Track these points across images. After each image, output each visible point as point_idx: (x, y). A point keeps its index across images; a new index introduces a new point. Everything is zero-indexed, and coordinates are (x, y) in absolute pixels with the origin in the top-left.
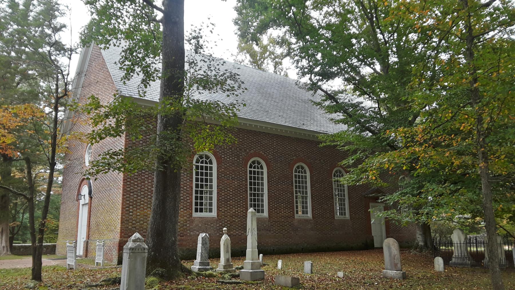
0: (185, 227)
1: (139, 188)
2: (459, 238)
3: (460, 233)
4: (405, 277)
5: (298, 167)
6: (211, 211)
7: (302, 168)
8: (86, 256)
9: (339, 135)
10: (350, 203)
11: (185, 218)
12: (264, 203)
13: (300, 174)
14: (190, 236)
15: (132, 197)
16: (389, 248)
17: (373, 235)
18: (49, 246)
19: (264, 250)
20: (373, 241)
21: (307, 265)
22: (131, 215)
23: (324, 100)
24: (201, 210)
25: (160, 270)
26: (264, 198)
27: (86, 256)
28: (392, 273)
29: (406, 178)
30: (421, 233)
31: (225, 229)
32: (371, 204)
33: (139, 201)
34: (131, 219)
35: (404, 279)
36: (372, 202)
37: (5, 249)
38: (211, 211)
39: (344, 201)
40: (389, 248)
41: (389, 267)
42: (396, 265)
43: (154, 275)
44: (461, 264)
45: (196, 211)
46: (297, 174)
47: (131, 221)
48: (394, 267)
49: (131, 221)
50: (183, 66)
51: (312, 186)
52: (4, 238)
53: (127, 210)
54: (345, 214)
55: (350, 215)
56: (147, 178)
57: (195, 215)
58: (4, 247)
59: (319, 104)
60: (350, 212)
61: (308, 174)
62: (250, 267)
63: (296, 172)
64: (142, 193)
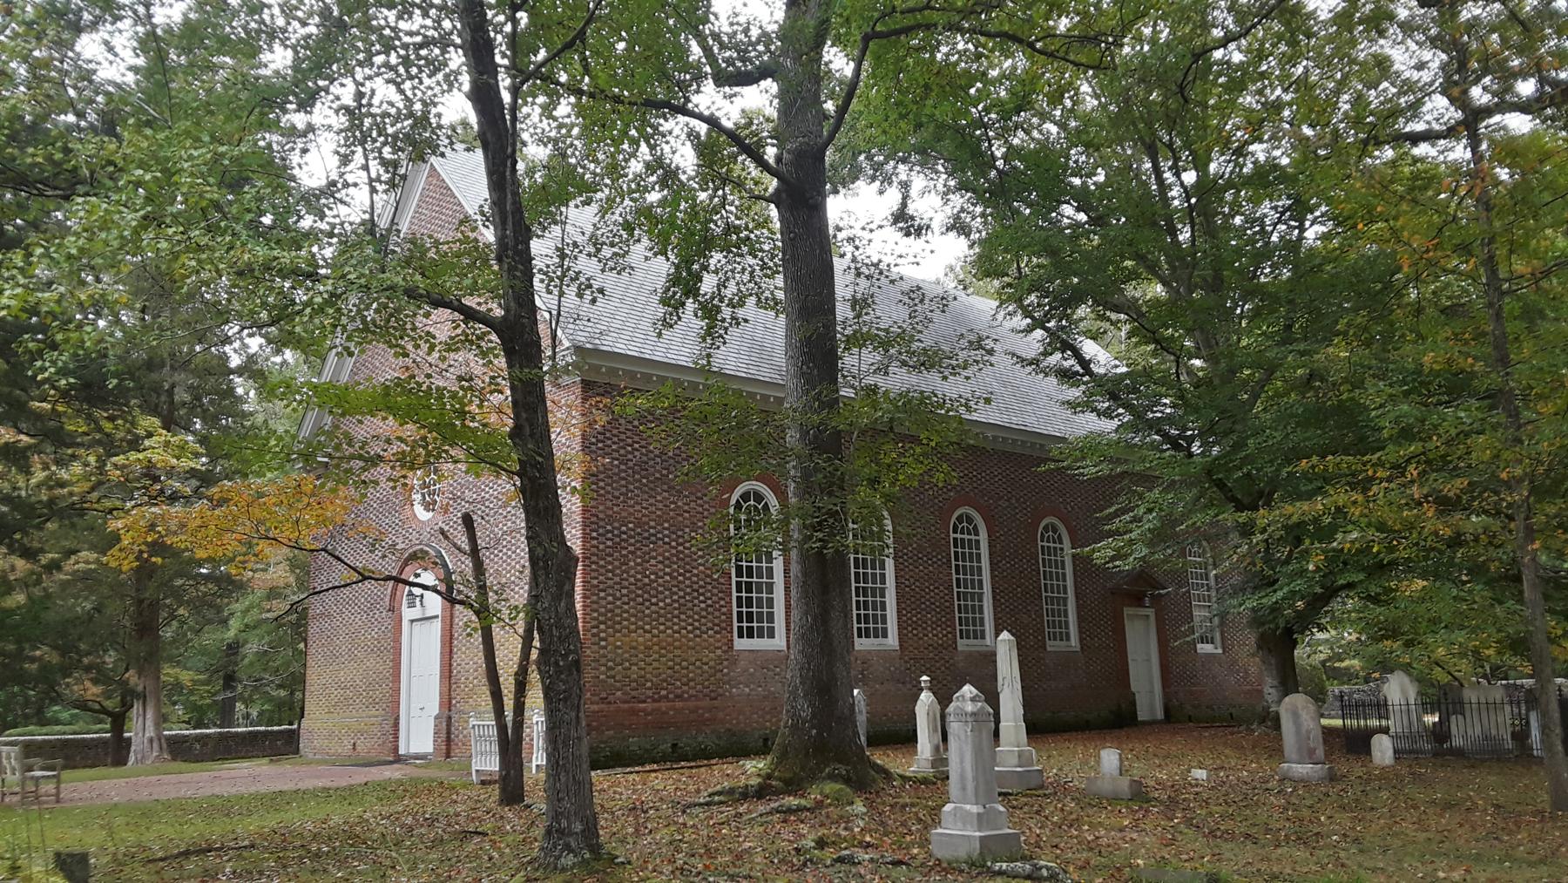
0: (719, 675)
1: (617, 579)
2: (1404, 692)
3: (1406, 680)
4: (1332, 778)
5: (960, 519)
6: (771, 635)
7: (970, 520)
8: (448, 756)
9: (1090, 446)
10: (1079, 608)
11: (719, 652)
12: (888, 612)
13: (966, 537)
14: (732, 696)
15: (603, 602)
16: (1295, 715)
17: (1134, 687)
18: (208, 736)
19: (1036, 728)
20: (1134, 704)
21: (1110, 758)
22: (605, 648)
23: (1046, 354)
24: (750, 636)
25: (843, 770)
26: (887, 600)
27: (448, 756)
28: (1302, 769)
29: (235, 361)
30: (1275, 683)
31: (925, 678)
32: (1127, 611)
33: (618, 611)
34: (604, 656)
35: (1331, 780)
36: (1130, 606)
37: (155, 745)
38: (771, 635)
39: (981, 600)
40: (1295, 715)
41: (1294, 756)
42: (1312, 752)
43: (832, 777)
44: (1411, 752)
45: (741, 636)
46: (959, 536)
47: (603, 661)
48: (1309, 756)
49: (603, 661)
50: (832, 311)
51: (993, 566)
52: (149, 715)
53: (594, 635)
54: (1068, 639)
55: (1081, 640)
56: (632, 553)
57: (741, 644)
58: (151, 740)
59: (1034, 362)
60: (1080, 632)
61: (983, 537)
62: (1015, 761)
63: (955, 532)
64: (624, 591)
